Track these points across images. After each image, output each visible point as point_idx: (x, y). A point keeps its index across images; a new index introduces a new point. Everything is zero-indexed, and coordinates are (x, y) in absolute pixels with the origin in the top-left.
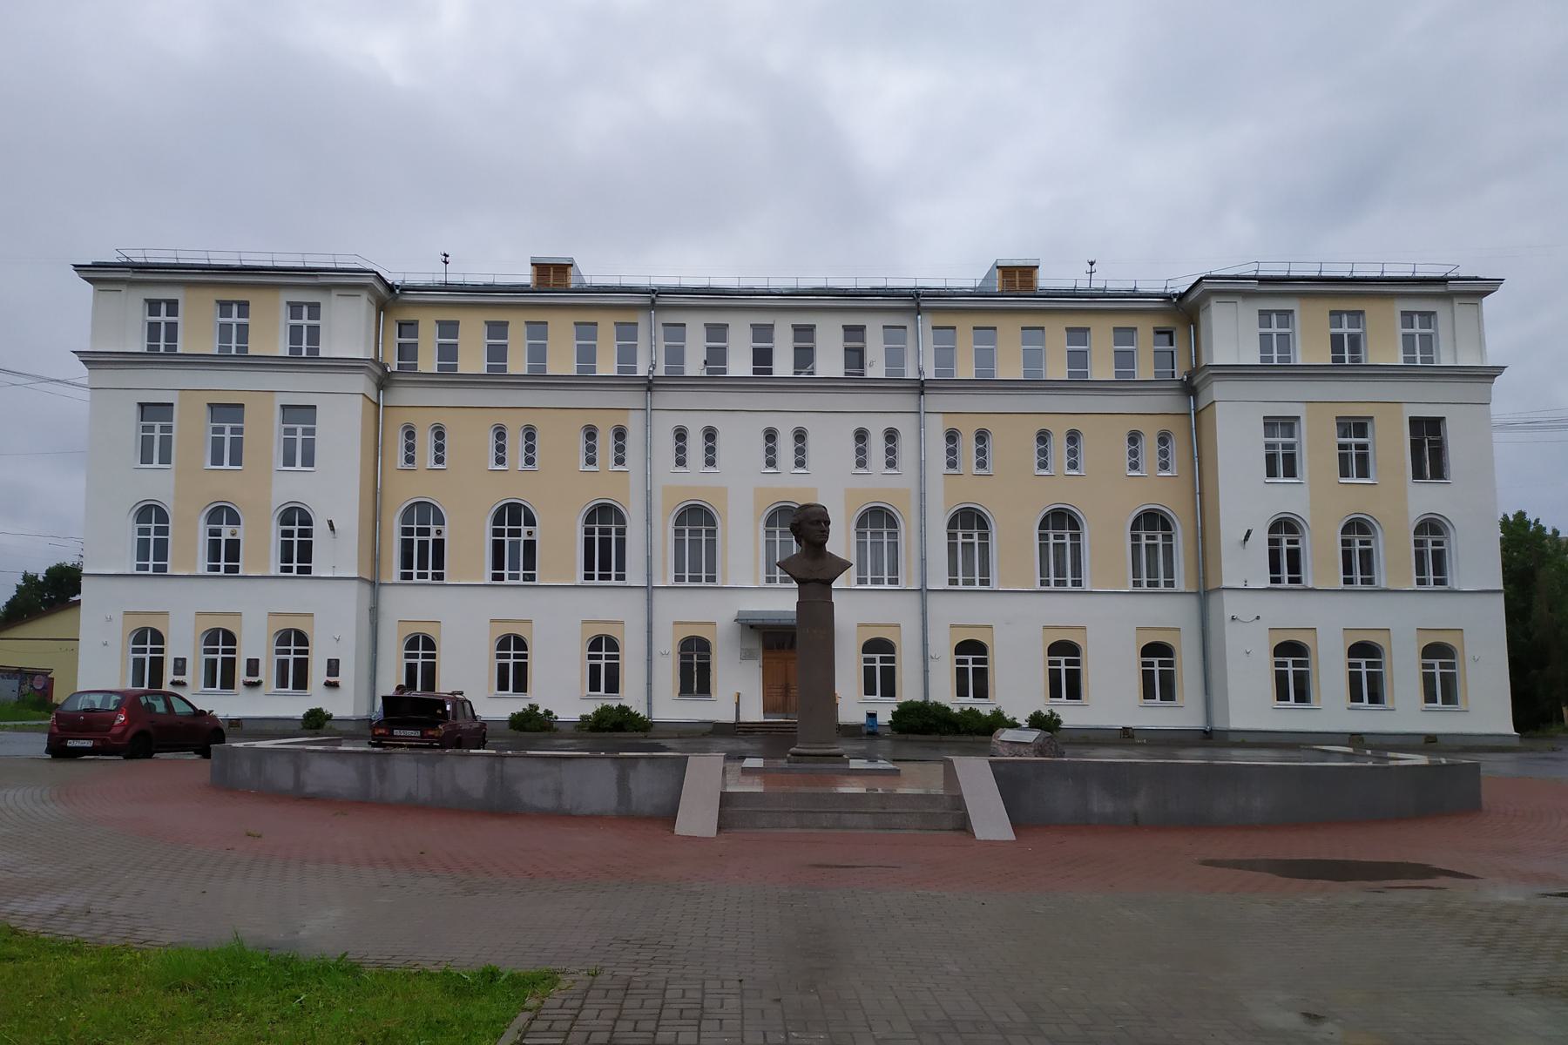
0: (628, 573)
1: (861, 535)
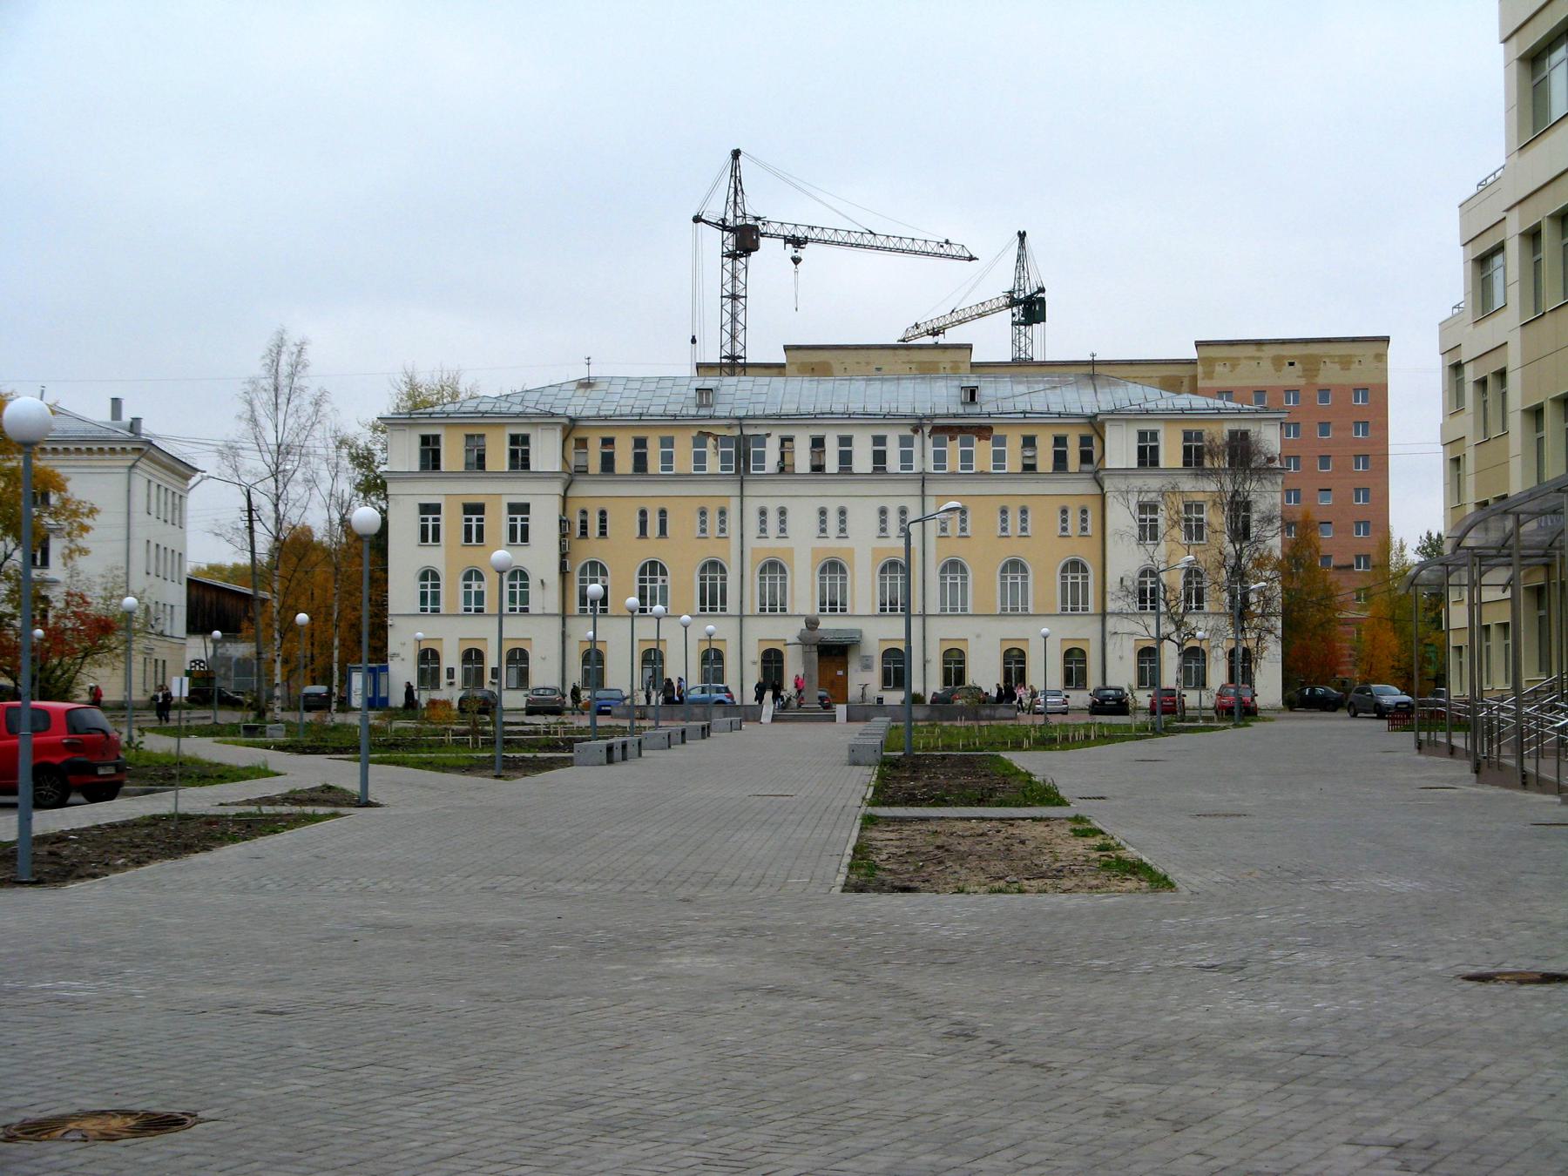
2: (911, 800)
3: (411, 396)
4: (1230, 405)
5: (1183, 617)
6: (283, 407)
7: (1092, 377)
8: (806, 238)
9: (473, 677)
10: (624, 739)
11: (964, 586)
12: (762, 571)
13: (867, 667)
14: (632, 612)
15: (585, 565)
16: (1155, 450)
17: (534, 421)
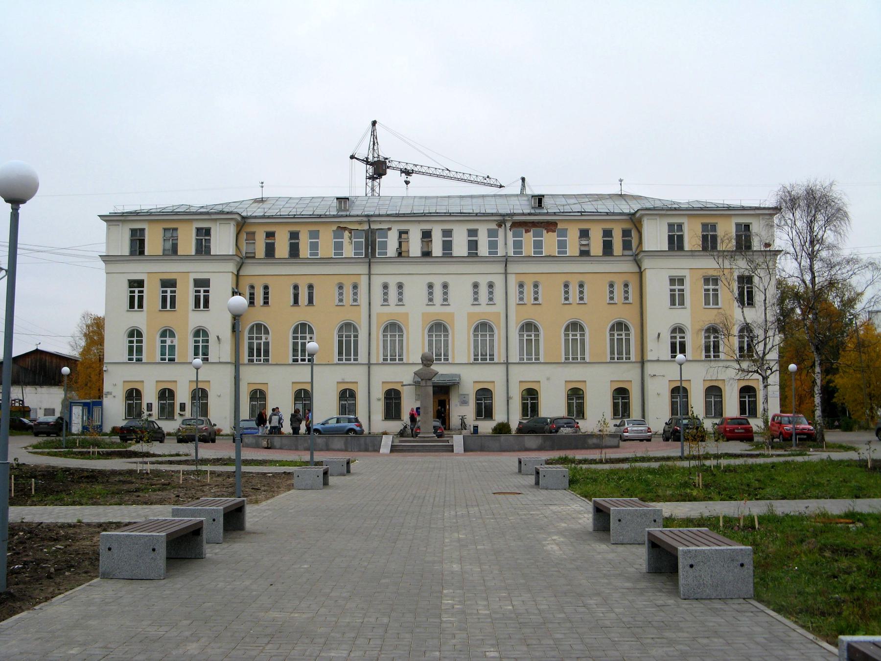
0: (359, 357)
1: (476, 336)
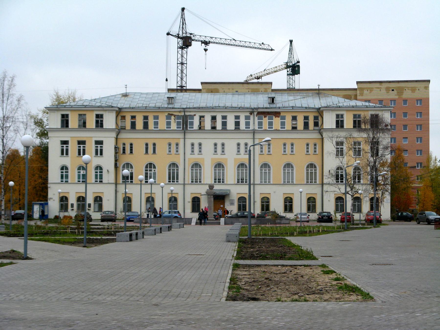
1: (238, 170)
2: (252, 257)
3: (57, 100)
4: (371, 104)
5: (353, 185)
6: (5, 101)
7: (318, 94)
8: (210, 41)
9: (81, 207)
10: (137, 231)
11: (269, 173)
12: (192, 167)
13: (232, 204)
14: (141, 181)
15: (124, 164)
16: (342, 122)
17: (105, 109)
